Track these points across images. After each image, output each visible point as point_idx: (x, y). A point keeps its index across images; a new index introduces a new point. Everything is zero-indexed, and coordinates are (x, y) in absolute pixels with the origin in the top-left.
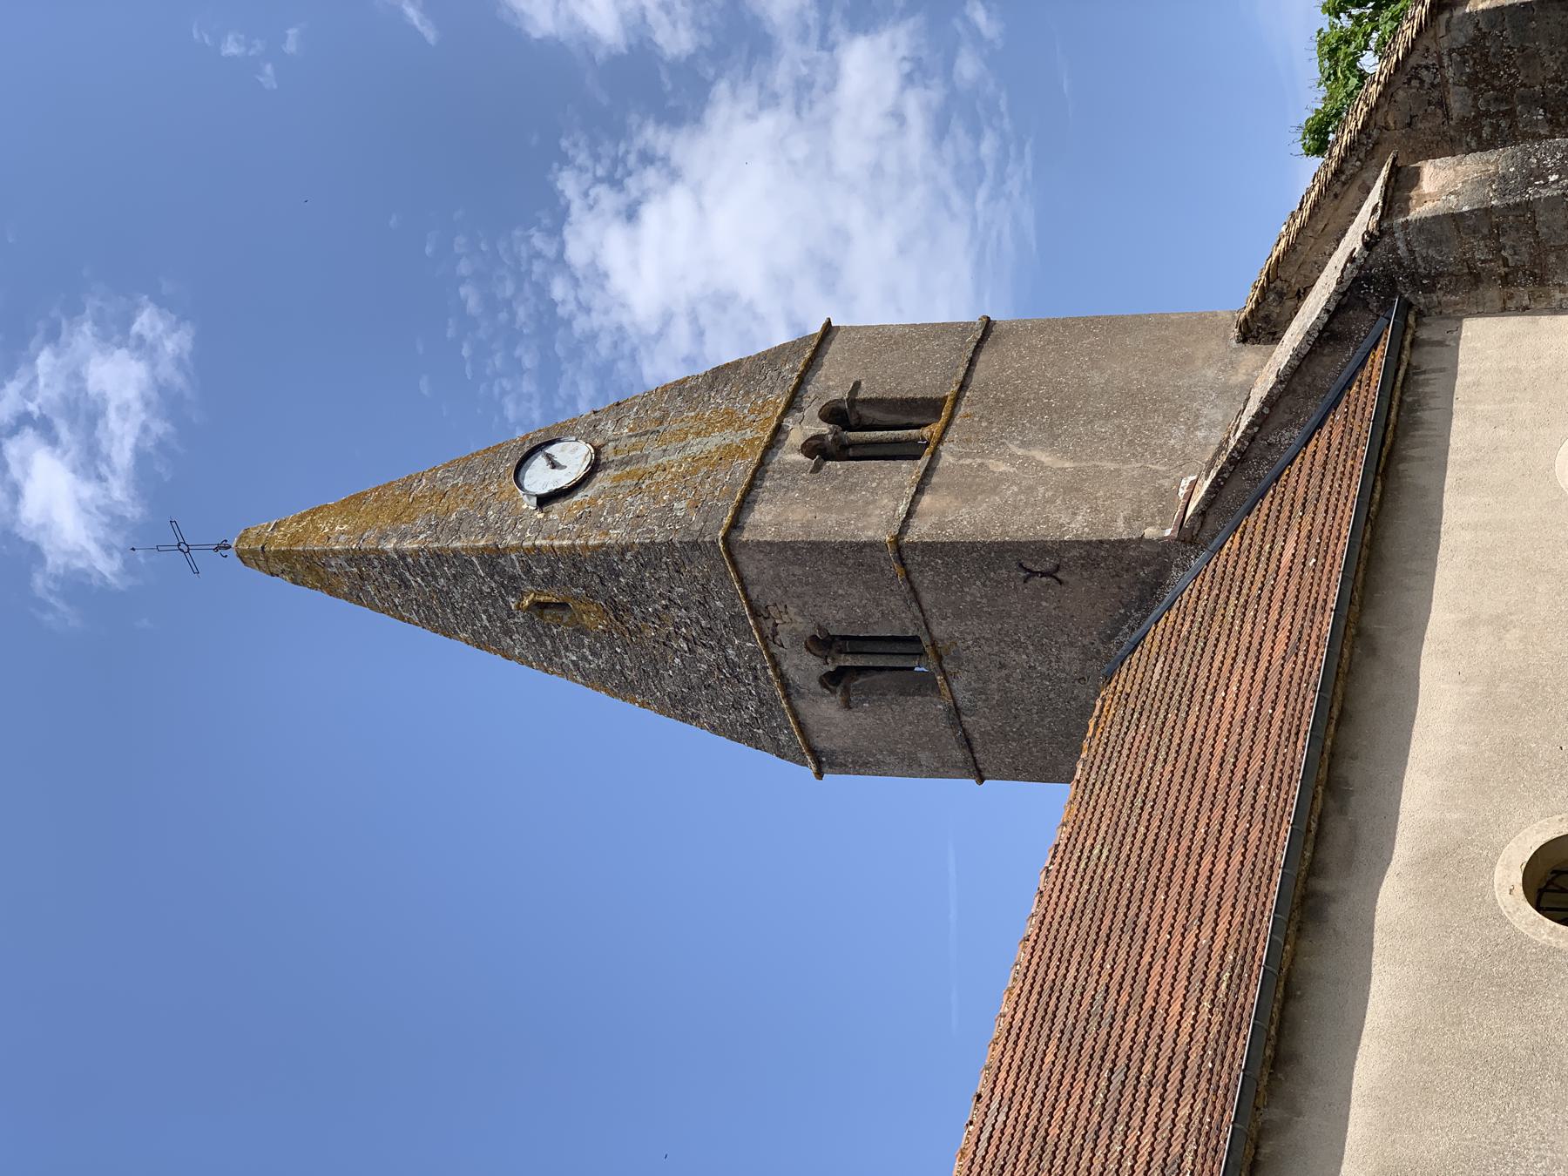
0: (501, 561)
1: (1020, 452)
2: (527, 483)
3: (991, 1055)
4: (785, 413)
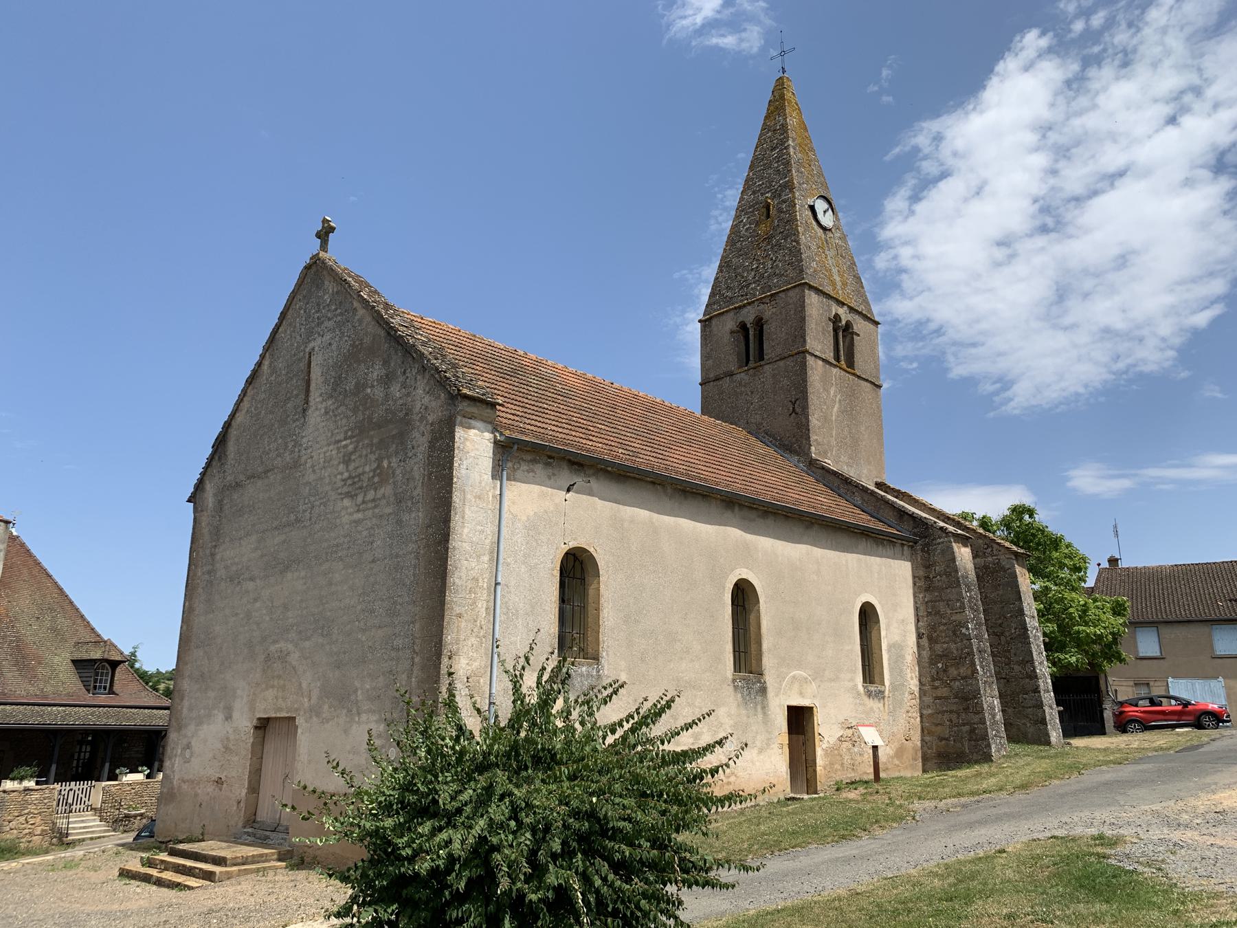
0: (788, 190)
1: (837, 399)
2: (818, 200)
3: (625, 388)
4: (849, 307)
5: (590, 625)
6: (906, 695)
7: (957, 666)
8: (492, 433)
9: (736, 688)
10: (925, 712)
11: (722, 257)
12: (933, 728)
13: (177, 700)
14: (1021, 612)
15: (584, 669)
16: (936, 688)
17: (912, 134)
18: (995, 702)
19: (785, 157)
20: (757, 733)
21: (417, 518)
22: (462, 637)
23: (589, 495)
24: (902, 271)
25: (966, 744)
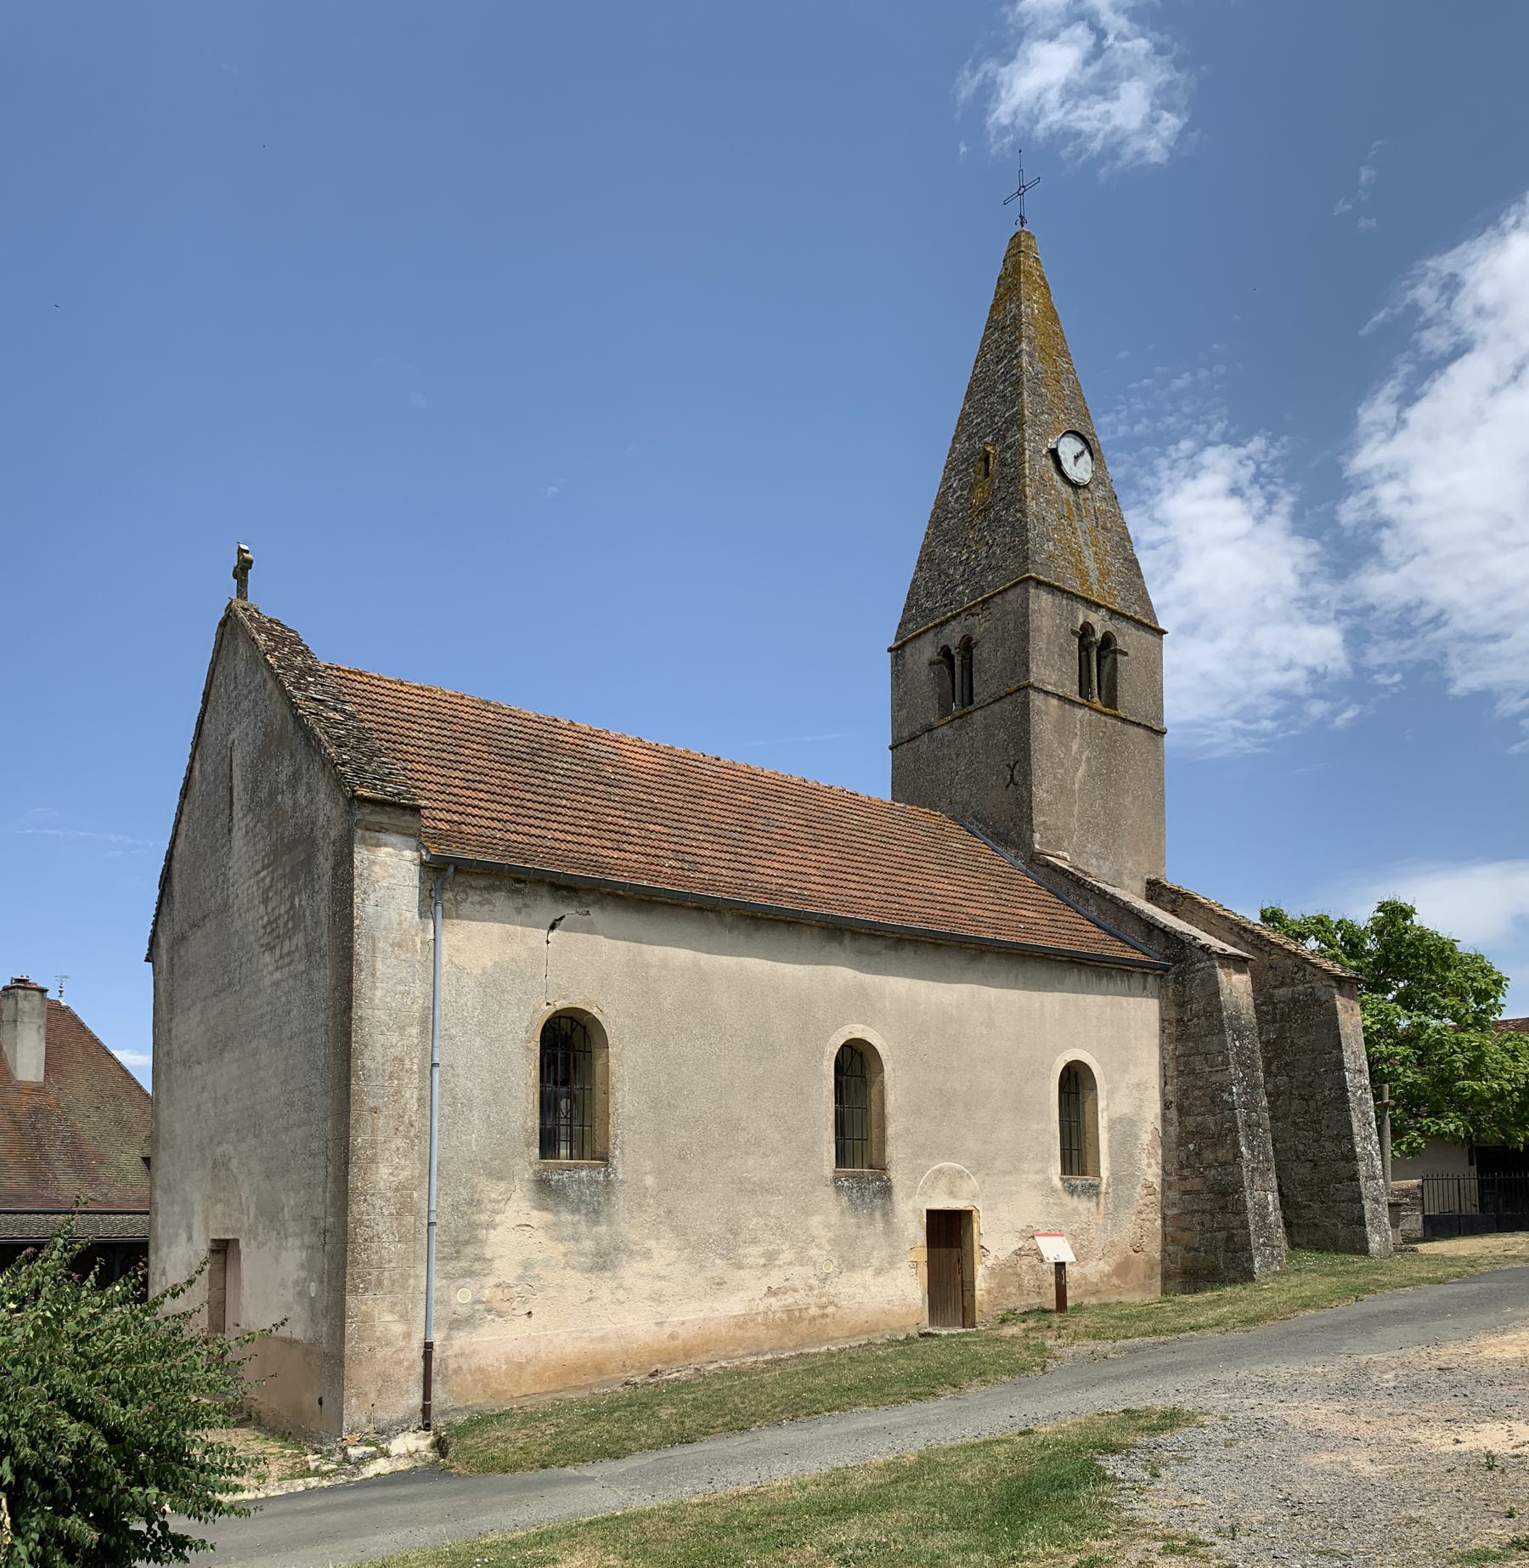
0: (1015, 428)
1: (1084, 757)
2: (1065, 439)
4: (1108, 609)
5: (597, 1113)
6: (1139, 1189)
7: (1214, 1147)
8: (418, 850)
9: (839, 1189)
10: (1169, 1212)
11: (923, 547)
12: (1179, 1234)
13: (153, 1216)
14: (1340, 1065)
15: (584, 1173)
16: (1185, 1178)
17: (1408, 282)
18: (1270, 1198)
19: (1014, 372)
20: (873, 1248)
21: (324, 976)
22: (381, 1138)
23: (588, 932)
24: (1386, 524)
25: (1221, 1255)
